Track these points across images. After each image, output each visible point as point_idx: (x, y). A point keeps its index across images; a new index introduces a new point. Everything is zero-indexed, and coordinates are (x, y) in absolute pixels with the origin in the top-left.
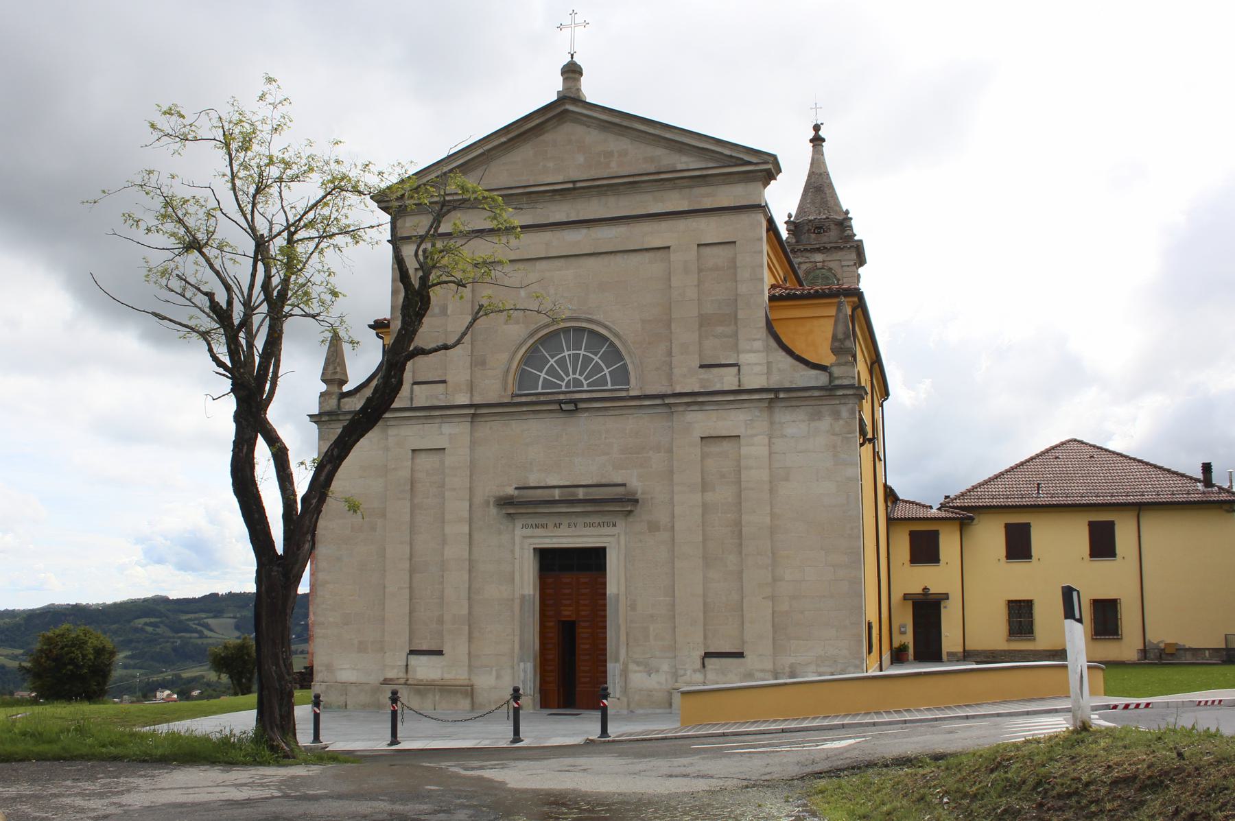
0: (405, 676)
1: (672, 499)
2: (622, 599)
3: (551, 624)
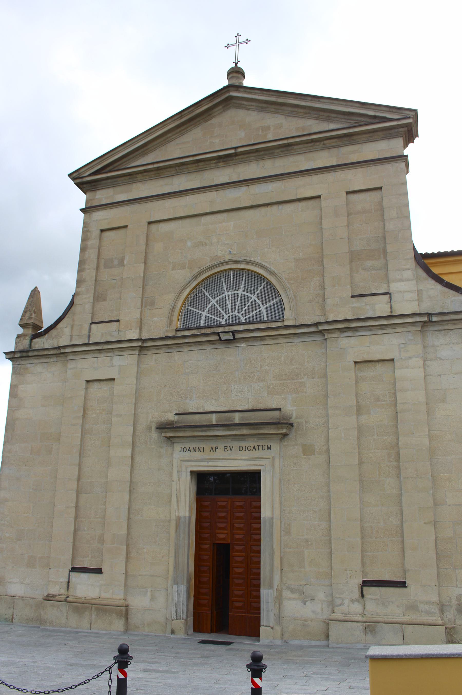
0: (66, 593)
1: (327, 422)
2: (277, 522)
3: (207, 546)
